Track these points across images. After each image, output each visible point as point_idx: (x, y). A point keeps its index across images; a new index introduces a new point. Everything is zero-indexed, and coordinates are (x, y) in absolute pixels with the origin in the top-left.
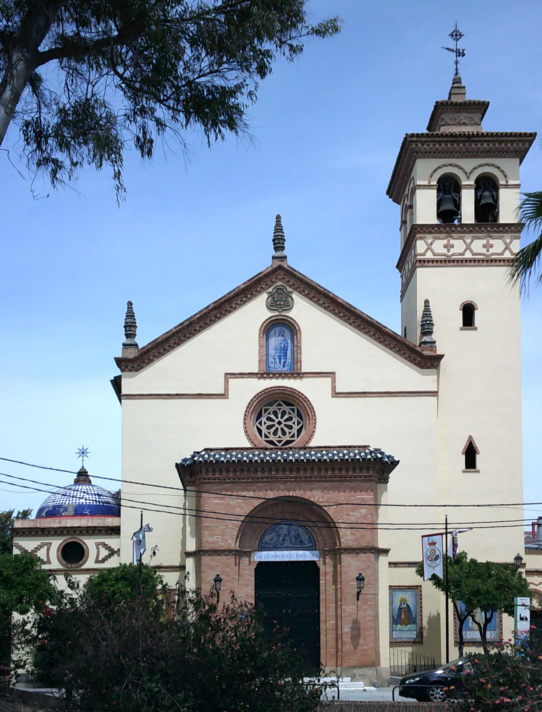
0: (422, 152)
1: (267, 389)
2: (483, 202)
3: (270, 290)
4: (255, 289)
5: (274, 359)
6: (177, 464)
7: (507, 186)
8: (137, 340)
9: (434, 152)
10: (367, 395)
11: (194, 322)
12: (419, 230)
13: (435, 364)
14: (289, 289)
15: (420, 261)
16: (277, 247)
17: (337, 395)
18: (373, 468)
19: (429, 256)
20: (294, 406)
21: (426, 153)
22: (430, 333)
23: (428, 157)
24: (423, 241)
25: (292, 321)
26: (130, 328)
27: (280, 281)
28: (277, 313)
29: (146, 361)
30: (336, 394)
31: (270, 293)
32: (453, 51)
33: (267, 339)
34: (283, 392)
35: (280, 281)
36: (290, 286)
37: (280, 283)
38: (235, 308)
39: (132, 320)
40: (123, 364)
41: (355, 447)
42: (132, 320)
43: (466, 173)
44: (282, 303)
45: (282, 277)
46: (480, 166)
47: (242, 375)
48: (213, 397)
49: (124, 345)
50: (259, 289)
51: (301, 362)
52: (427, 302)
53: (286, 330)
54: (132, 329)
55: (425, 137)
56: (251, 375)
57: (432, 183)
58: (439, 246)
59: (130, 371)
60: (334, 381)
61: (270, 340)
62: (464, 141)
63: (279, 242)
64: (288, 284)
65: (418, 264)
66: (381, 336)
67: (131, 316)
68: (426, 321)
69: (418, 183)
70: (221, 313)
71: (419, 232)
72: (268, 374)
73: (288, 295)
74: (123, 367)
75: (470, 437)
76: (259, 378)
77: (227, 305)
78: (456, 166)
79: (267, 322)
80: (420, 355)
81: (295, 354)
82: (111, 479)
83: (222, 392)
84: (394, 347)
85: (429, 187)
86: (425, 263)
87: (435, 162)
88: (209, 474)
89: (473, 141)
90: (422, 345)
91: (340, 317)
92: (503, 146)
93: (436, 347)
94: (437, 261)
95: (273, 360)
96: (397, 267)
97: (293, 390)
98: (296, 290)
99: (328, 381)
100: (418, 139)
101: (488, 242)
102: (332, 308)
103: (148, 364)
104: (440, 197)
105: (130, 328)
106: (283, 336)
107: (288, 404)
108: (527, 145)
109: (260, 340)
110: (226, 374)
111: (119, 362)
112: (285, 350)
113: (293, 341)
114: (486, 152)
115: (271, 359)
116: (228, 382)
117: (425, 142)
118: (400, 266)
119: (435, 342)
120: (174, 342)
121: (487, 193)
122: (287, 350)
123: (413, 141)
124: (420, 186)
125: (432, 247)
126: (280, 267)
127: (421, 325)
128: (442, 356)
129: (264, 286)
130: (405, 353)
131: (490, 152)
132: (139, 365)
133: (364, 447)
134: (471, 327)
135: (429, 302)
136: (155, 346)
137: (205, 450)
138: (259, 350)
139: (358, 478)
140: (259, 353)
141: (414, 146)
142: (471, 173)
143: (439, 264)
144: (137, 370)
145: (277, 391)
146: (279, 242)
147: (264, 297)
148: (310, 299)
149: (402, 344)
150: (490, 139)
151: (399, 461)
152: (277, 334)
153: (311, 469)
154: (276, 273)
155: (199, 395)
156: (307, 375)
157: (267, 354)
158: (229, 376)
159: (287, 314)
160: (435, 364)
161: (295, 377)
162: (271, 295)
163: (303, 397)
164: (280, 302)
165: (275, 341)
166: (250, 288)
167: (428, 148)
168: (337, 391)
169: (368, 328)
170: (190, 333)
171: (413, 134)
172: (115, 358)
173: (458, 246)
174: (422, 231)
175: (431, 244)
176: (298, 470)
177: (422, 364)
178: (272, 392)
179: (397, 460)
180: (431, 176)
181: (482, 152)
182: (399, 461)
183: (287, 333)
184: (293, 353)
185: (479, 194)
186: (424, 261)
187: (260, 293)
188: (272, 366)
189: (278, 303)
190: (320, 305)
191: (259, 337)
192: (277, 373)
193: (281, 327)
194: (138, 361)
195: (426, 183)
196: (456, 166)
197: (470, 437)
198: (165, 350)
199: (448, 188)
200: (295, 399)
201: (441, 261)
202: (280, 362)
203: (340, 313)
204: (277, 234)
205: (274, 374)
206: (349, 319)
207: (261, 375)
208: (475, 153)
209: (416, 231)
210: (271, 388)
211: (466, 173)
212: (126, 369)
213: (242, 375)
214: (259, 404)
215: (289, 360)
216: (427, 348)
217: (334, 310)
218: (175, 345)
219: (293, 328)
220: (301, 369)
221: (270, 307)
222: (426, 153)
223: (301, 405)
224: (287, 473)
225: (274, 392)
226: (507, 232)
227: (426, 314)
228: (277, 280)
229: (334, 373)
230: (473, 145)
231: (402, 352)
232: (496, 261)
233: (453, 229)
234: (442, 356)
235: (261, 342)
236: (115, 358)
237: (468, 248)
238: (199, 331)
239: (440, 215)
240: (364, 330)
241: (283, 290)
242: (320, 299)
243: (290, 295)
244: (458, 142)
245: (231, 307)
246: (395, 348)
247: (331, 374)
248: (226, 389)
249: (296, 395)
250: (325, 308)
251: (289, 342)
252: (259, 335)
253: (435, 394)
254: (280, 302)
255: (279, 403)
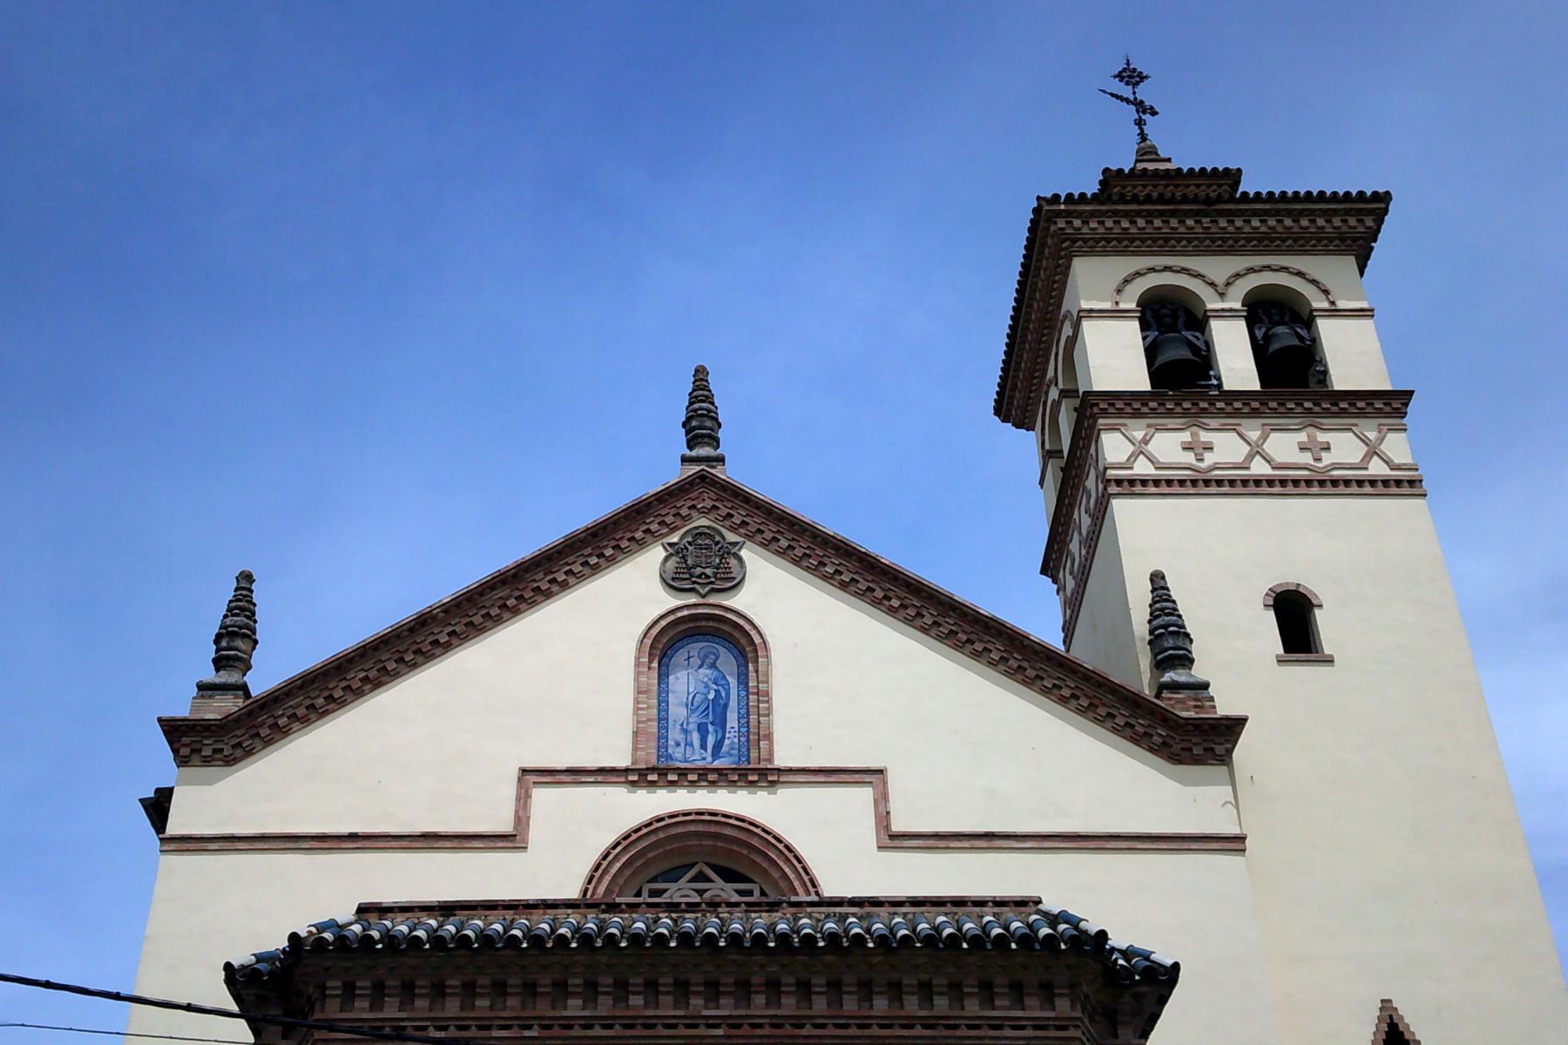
0: (1085, 241)
1: (660, 820)
2: (1275, 346)
3: (675, 539)
4: (629, 535)
5: (685, 732)
6: (228, 967)
7: (1334, 312)
8: (249, 679)
9: (1119, 241)
10: (997, 843)
11: (434, 618)
12: (1103, 405)
13: (1220, 750)
14: (731, 537)
15: (1119, 482)
16: (697, 436)
17: (896, 843)
18: (1072, 986)
19: (1143, 468)
20: (751, 881)
21: (1098, 241)
22: (1187, 661)
23: (1104, 253)
24: (1118, 435)
25: (741, 622)
26: (236, 637)
27: (704, 515)
28: (693, 599)
29: (264, 732)
30: (893, 837)
31: (671, 545)
32: (1127, 101)
33: (663, 676)
34: (713, 829)
35: (704, 515)
36: (732, 529)
37: (704, 522)
38: (565, 586)
39: (241, 620)
40: (185, 740)
41: (980, 903)
42: (241, 620)
43: (1212, 284)
44: (709, 571)
45: (709, 504)
46: (1138, 274)
47: (576, 775)
48: (476, 844)
49: (202, 687)
50: (639, 535)
51: (769, 737)
52: (1157, 580)
53: (722, 650)
54: (239, 643)
55: (1089, 202)
56: (605, 775)
57: (1122, 306)
58: (1169, 446)
59: (207, 762)
60: (882, 799)
61: (671, 678)
62: (1197, 213)
63: (701, 424)
64: (727, 523)
65: (1113, 489)
66: (1025, 664)
67: (243, 609)
68: (1165, 627)
69: (1085, 305)
70: (520, 598)
71: (1105, 413)
72: (663, 772)
73: (730, 551)
74: (184, 751)
75: (1386, 1004)
76: (633, 783)
77: (541, 575)
78: (1184, 270)
79: (663, 623)
80: (1166, 719)
81: (753, 717)
82: (48, 985)
83: (506, 827)
84: (1073, 696)
85: (1116, 314)
86: (1134, 486)
87: (1126, 265)
88: (358, 1004)
89: (1221, 213)
90: (1165, 694)
91: (892, 611)
92: (1304, 222)
93: (1212, 699)
94: (1169, 482)
95: (680, 737)
96: (1043, 572)
97: (746, 826)
98: (750, 537)
99: (863, 796)
100: (1072, 208)
101: (1311, 438)
102: (863, 585)
103: (268, 742)
104: (1149, 340)
105: (236, 637)
106: (713, 666)
107: (729, 876)
108: (1369, 222)
109: (638, 674)
110: (524, 771)
111: (174, 730)
112: (717, 710)
113: (743, 680)
114: (1260, 240)
115: (675, 734)
116: (528, 796)
117: (1093, 214)
118: (1050, 567)
119: (1205, 686)
120: (363, 674)
121: (1281, 330)
122: (726, 706)
123: (1059, 214)
124: (1091, 311)
125: (1149, 447)
126: (702, 478)
127: (1150, 642)
128: (1240, 722)
129: (654, 527)
130: (1111, 716)
131: (1272, 240)
132: (239, 744)
133: (1021, 903)
134: (1312, 656)
135: (1163, 578)
136: (301, 688)
137: (363, 910)
138: (637, 702)
139: (1008, 1032)
140: (637, 709)
141: (1061, 224)
142: (1228, 284)
143: (1176, 489)
144: (230, 761)
145: (693, 828)
146: (701, 424)
147: (655, 555)
148: (796, 562)
149: (1100, 685)
150: (1268, 206)
151: (1176, 966)
152: (696, 661)
153: (799, 984)
154: (693, 495)
155: (425, 836)
156: (791, 778)
157: (663, 720)
158: (532, 778)
159: (726, 603)
160: (1220, 750)
161: (752, 784)
162: (675, 550)
163: (781, 846)
164: (703, 568)
165: (686, 682)
166: (614, 531)
167: (1102, 230)
168: (897, 827)
169: (981, 640)
170: (418, 652)
171: (1056, 197)
172: (160, 720)
173: (1226, 447)
174: (1112, 410)
175: (1146, 441)
176: (744, 989)
177: (1176, 748)
178: (674, 831)
179: (1169, 962)
180: (1119, 291)
181: (1249, 240)
182: (1176, 966)
183: (727, 662)
184: (744, 717)
185: (1259, 333)
186: (1132, 482)
187: (641, 544)
188: (678, 753)
189: (698, 570)
190: (826, 578)
191: (638, 664)
192: (692, 770)
193: (704, 635)
194: (238, 733)
195: (1107, 305)
196: (1184, 270)
197: (1386, 1004)
198: (330, 699)
199: (1171, 323)
200: (754, 857)
201: (1182, 483)
202: (704, 746)
203: (890, 599)
204: (696, 406)
205: (682, 773)
206: (919, 615)
207: (639, 776)
208: (1231, 242)
209: (1095, 410)
210: (671, 816)
211: (1212, 284)
212: (195, 759)
213: (576, 775)
214: (628, 872)
215: (731, 737)
216: (1179, 701)
217: (870, 589)
218: (368, 687)
219: (743, 641)
220: (770, 760)
221: (672, 583)
222: (1098, 241)
223: (776, 875)
224: (697, 1002)
225: (680, 830)
226: (1362, 414)
227: (1162, 610)
228: (694, 513)
229: (881, 772)
230: (1223, 223)
231: (1102, 711)
232: (1347, 482)
233: (1203, 405)
234: (1240, 722)
235: (643, 679)
236: (160, 720)
237: (1256, 451)
238: (447, 647)
239: (1157, 374)
240: (968, 646)
241: (711, 537)
242: (825, 560)
243: (735, 550)
244: (1182, 216)
245: (553, 581)
246: (1078, 698)
247: (873, 776)
248: (522, 819)
249: (755, 842)
250: (844, 586)
251: (733, 682)
252: (637, 658)
253: (1234, 843)
254: (703, 568)
255: (701, 872)
